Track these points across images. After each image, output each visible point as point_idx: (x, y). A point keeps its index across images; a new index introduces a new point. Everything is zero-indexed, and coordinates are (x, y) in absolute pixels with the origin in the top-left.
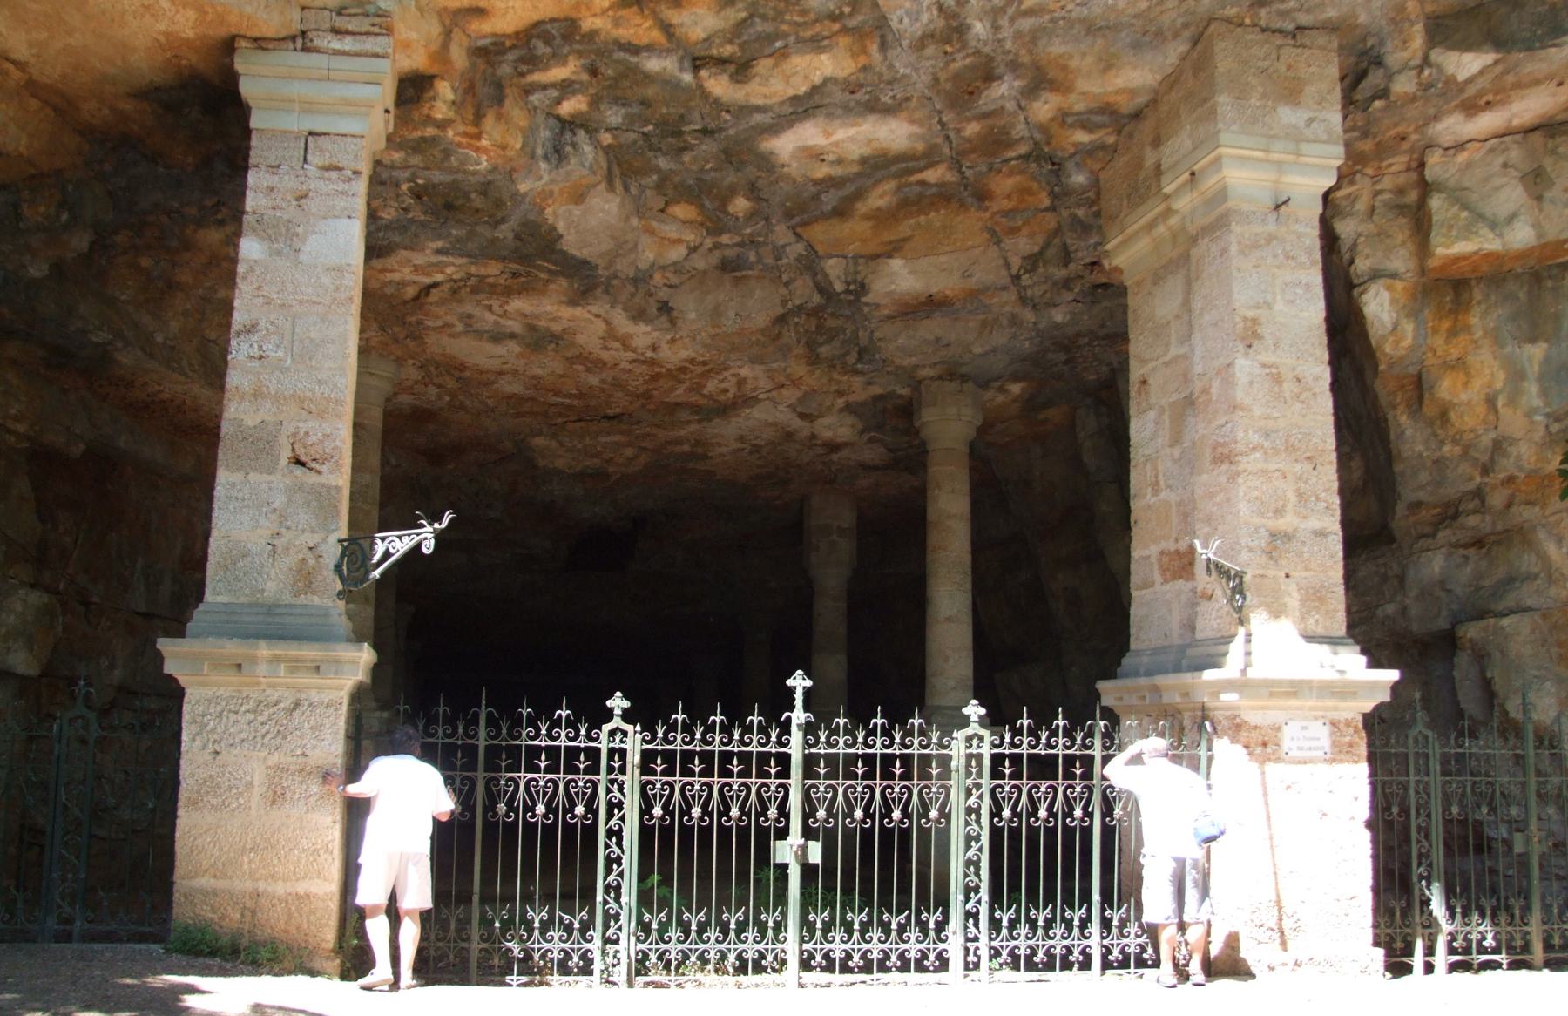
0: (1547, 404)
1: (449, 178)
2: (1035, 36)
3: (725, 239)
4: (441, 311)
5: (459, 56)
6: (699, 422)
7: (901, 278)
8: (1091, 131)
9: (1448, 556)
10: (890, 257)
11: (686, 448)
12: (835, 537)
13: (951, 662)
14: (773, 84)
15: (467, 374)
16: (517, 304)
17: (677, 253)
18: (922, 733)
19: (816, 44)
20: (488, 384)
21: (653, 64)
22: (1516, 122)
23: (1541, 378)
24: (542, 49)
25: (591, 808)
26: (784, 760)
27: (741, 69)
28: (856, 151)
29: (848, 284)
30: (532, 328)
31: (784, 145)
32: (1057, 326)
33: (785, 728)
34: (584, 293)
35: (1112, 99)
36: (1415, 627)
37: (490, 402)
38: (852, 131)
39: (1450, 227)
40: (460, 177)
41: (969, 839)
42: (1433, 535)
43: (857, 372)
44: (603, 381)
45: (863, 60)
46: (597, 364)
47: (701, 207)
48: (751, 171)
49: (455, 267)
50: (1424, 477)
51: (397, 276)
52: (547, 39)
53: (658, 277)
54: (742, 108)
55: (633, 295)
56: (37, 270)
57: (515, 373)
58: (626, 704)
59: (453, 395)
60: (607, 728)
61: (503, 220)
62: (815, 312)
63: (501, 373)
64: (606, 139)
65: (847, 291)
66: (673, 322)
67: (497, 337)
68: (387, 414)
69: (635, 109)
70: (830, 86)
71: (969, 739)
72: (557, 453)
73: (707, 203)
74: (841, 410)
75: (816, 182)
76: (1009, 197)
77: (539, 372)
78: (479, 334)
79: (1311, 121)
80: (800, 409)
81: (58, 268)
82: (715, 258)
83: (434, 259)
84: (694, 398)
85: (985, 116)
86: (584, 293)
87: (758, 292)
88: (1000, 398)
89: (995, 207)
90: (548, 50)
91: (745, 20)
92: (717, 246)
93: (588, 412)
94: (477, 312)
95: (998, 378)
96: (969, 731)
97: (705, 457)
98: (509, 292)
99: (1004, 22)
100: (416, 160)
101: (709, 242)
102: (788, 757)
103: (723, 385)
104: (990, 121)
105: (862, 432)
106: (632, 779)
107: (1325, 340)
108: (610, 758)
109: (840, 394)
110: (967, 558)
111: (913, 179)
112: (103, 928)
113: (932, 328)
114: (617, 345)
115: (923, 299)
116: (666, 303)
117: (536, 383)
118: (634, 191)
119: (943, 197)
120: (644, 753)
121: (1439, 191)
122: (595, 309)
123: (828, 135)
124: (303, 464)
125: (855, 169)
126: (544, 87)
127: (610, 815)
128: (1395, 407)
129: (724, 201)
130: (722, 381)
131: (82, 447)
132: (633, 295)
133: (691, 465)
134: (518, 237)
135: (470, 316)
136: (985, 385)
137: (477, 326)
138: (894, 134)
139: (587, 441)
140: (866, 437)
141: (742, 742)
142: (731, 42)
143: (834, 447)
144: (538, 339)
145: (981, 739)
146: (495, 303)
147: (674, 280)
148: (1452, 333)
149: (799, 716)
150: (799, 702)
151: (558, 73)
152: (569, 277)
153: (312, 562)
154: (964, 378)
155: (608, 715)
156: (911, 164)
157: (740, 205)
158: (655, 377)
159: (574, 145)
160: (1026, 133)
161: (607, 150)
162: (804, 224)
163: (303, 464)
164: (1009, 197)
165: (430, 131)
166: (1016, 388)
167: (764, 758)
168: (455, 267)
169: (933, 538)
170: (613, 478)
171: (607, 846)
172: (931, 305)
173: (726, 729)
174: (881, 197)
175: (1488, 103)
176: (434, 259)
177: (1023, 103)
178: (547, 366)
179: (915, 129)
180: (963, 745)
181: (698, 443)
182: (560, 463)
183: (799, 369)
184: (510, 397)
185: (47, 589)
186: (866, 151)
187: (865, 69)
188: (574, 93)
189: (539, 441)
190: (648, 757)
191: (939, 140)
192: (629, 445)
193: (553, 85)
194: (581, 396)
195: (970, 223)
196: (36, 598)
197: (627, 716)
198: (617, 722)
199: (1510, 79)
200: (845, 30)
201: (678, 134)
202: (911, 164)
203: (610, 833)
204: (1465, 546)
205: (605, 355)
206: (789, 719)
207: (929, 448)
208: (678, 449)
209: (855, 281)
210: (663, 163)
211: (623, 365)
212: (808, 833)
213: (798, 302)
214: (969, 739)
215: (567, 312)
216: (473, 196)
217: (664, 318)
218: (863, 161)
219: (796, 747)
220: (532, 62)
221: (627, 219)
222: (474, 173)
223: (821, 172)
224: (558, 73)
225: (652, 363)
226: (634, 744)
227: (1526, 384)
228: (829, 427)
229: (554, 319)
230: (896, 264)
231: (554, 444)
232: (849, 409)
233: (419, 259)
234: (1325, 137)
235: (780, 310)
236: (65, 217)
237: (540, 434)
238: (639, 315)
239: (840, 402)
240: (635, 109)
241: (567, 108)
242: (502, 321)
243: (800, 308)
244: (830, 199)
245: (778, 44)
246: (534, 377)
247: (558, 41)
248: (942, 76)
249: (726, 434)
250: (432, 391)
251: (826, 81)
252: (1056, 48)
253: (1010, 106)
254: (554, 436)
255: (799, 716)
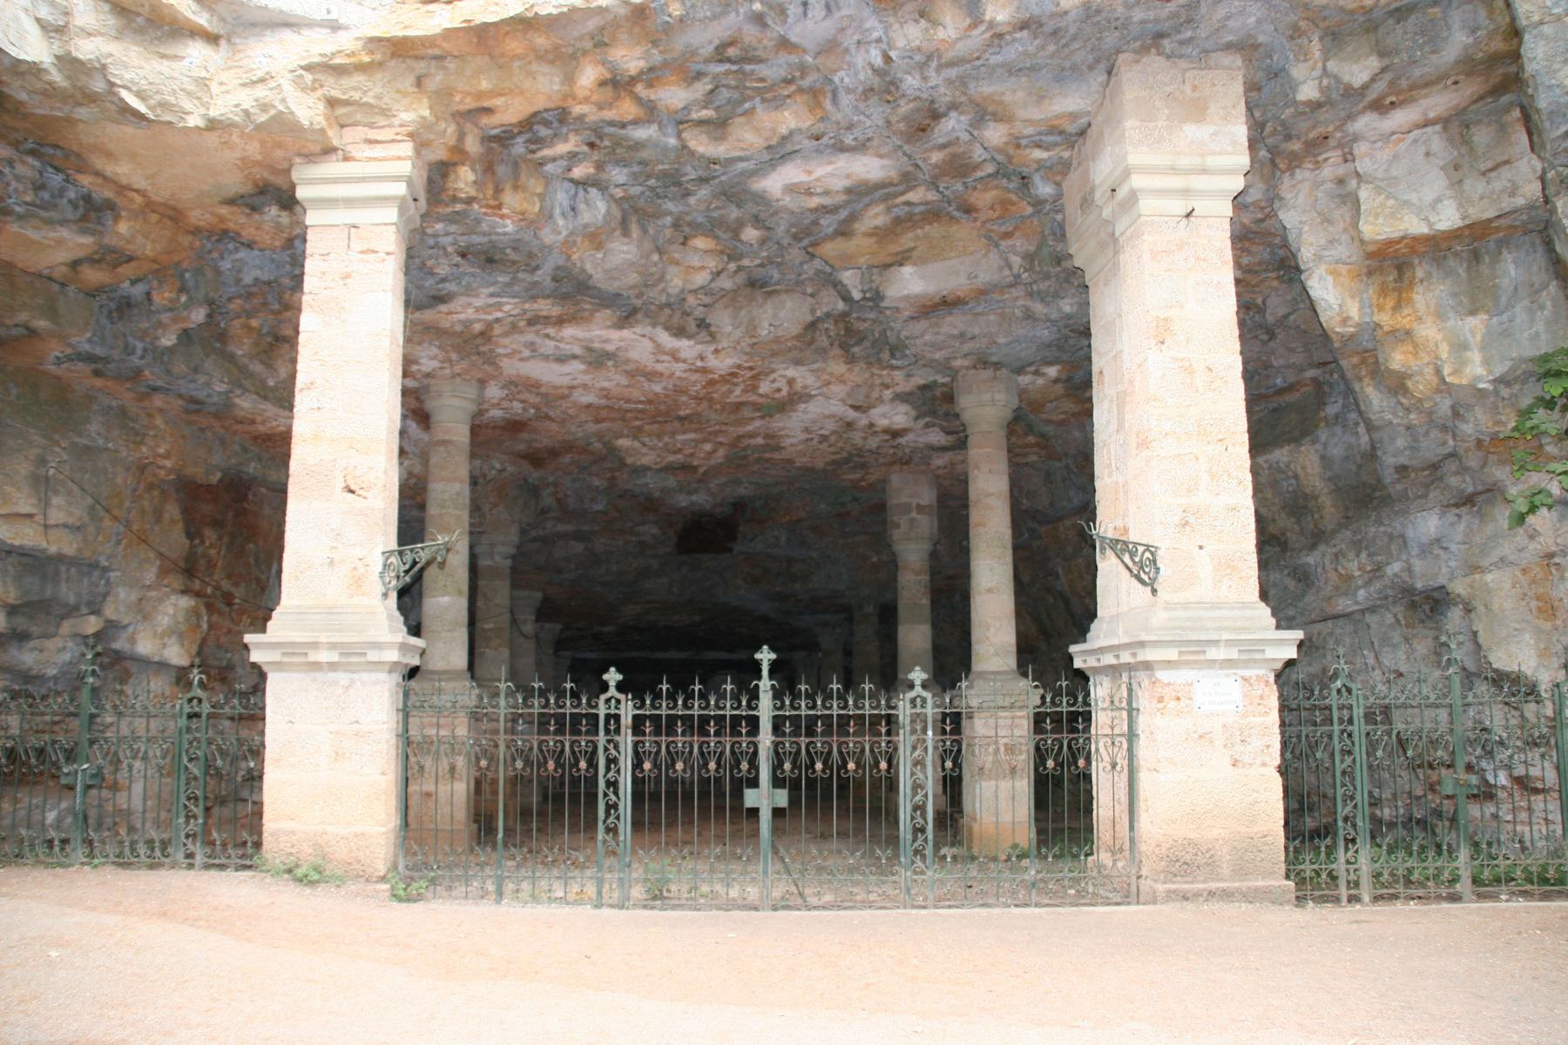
0: (1490, 372)
1: (485, 240)
2: (962, 81)
3: (746, 262)
4: (506, 341)
5: (472, 145)
6: (762, 417)
7: (910, 283)
8: (1047, 149)
9: (1443, 514)
10: (901, 265)
11: (760, 441)
12: (914, 514)
13: (992, 630)
14: (747, 138)
15: (543, 390)
16: (569, 331)
17: (701, 279)
18: (808, 696)
19: (777, 103)
20: (563, 397)
21: (640, 133)
22: (1432, 115)
23: (1484, 347)
24: (543, 132)
25: (592, 764)
26: (754, 723)
27: (718, 126)
28: (839, 184)
29: (864, 292)
30: (590, 350)
31: (774, 184)
32: (1068, 317)
33: (754, 695)
34: (627, 318)
35: (1055, 123)
36: (1419, 585)
37: (571, 412)
38: (830, 168)
39: (1377, 216)
40: (494, 237)
41: (916, 787)
42: (1425, 496)
43: (894, 368)
44: (665, 388)
45: (819, 114)
46: (651, 376)
47: (716, 237)
48: (751, 208)
49: (510, 306)
50: (1400, 443)
51: (462, 317)
52: (547, 124)
53: (691, 300)
54: (726, 160)
55: (671, 316)
56: (168, 340)
57: (585, 386)
58: (620, 677)
59: (537, 408)
60: (603, 697)
61: (537, 268)
62: (844, 316)
63: (573, 387)
64: (619, 193)
65: (864, 299)
66: (713, 337)
67: (561, 359)
68: (475, 430)
69: (636, 169)
70: (796, 138)
71: (913, 701)
72: (643, 452)
73: (721, 234)
74: (893, 400)
75: (811, 210)
76: (992, 208)
77: (606, 384)
78: (546, 358)
79: (1215, 134)
80: (850, 402)
81: (186, 336)
82: (740, 278)
83: (492, 301)
84: (753, 398)
85: (943, 146)
86: (627, 318)
87: (789, 304)
88: (1040, 381)
89: (982, 217)
90: (550, 132)
91: (712, 91)
92: (740, 269)
93: (662, 415)
94: (538, 340)
95: (1030, 364)
96: (609, 695)
97: (779, 448)
98: (560, 322)
99: (931, 72)
100: (453, 228)
101: (732, 266)
102: (756, 718)
103: (776, 385)
104: (947, 151)
105: (916, 418)
106: (627, 740)
107: (1236, 332)
108: (607, 722)
109: (887, 387)
110: (1007, 533)
111: (898, 201)
112: (217, 861)
113: (954, 323)
114: (667, 358)
115: (937, 300)
116: (703, 320)
117: (606, 394)
118: (651, 231)
119: (933, 214)
120: (635, 717)
121: (1368, 182)
122: (638, 330)
123: (810, 173)
124: (352, 492)
125: (844, 197)
126: (554, 160)
127: (608, 769)
128: (1360, 379)
129: (736, 229)
130: (773, 381)
131: (219, 475)
132: (671, 316)
133: (767, 455)
134: (555, 279)
135: (532, 344)
136: (1020, 371)
137: (542, 350)
138: (870, 168)
139: (666, 439)
140: (922, 422)
141: (718, 707)
142: (705, 107)
143: (896, 434)
144: (597, 359)
145: (924, 700)
146: (551, 331)
147: (707, 300)
148: (1397, 307)
149: (765, 684)
150: (765, 672)
151: (562, 148)
152: (607, 307)
153: (362, 570)
154: (997, 366)
155: (605, 687)
156: (891, 189)
157: (751, 234)
158: (711, 383)
159: (587, 201)
160: (986, 156)
161: (618, 201)
162: (813, 245)
163: (352, 492)
164: (992, 208)
165: (459, 207)
166: (1052, 371)
167: (736, 720)
168: (510, 306)
169: (975, 516)
170: (701, 470)
171: (606, 795)
172: (947, 304)
173: (672, 697)
174: (876, 217)
175: (1392, 103)
176: (492, 301)
177: (975, 133)
178: (612, 380)
179: (886, 162)
180: (908, 705)
181: (767, 436)
182: (647, 460)
183: (839, 368)
184: (589, 406)
185: (198, 594)
186: (847, 183)
187: (822, 119)
188: (580, 161)
189: (623, 443)
190: (638, 722)
191: (911, 169)
192: (705, 441)
193: (562, 157)
194: (650, 402)
195: (963, 231)
196: (185, 602)
197: (621, 687)
198: (918, 690)
199: (1404, 83)
200: (801, 90)
201: (678, 184)
202: (891, 189)
203: (609, 784)
204: (1457, 505)
205: (659, 367)
206: (757, 686)
207: (969, 432)
208: (753, 442)
209: (870, 290)
210: (670, 206)
211: (678, 374)
212: (777, 782)
213: (825, 310)
214: (913, 701)
215: (615, 335)
216: (508, 251)
217: (704, 333)
218: (848, 191)
219: (765, 708)
220: (538, 142)
221: (648, 257)
222: (505, 234)
223: (814, 202)
224: (562, 148)
225: (704, 370)
226: (627, 711)
227: (1468, 354)
228: (884, 416)
229: (606, 341)
230: (907, 270)
231: (637, 444)
232: (901, 398)
233: (479, 302)
234: (1230, 149)
235: (809, 318)
236: (183, 299)
237: (622, 436)
238: (680, 332)
239: (888, 394)
240: (636, 169)
241: (577, 172)
242: (562, 346)
243: (828, 315)
244: (828, 223)
245: (747, 105)
246: (602, 389)
247: (555, 124)
248: (894, 119)
249: (793, 428)
250: (517, 406)
251: (791, 133)
252: (987, 89)
253: (965, 137)
254: (635, 437)
255: (765, 684)
